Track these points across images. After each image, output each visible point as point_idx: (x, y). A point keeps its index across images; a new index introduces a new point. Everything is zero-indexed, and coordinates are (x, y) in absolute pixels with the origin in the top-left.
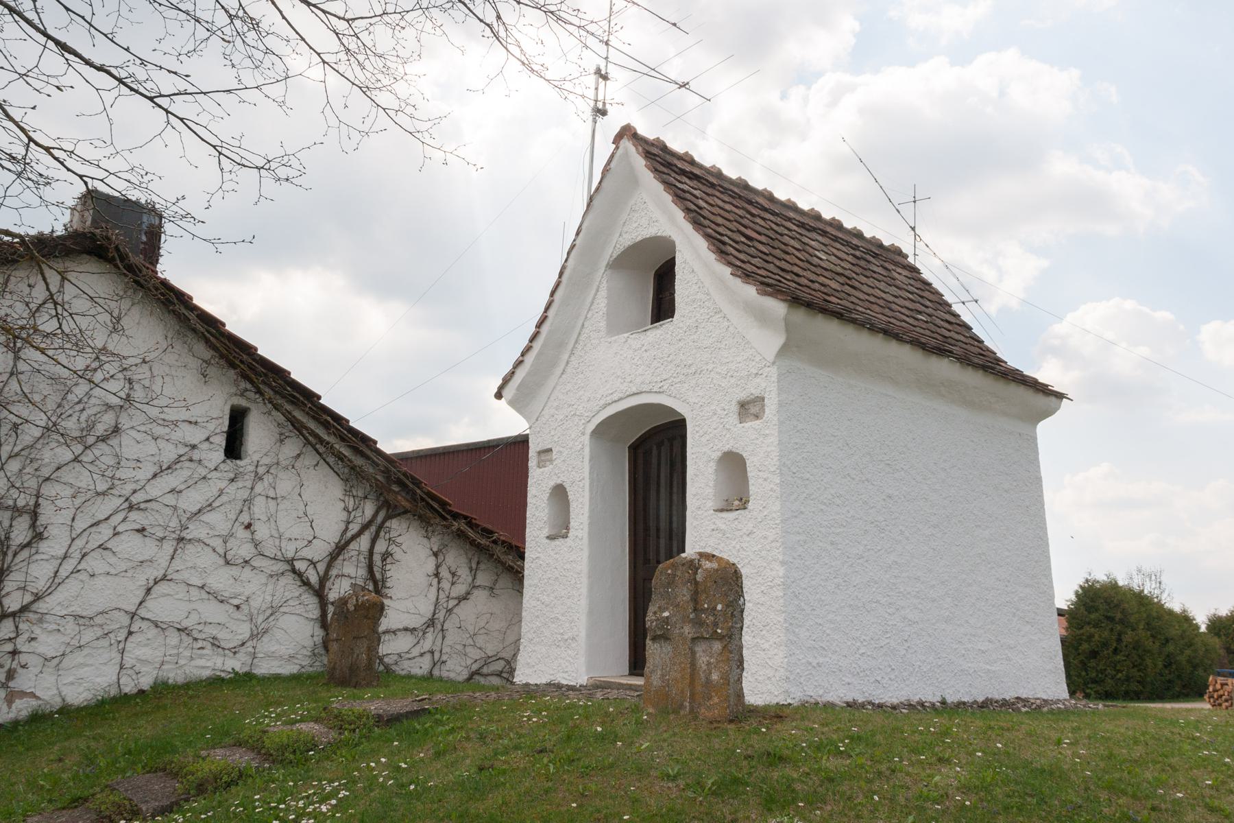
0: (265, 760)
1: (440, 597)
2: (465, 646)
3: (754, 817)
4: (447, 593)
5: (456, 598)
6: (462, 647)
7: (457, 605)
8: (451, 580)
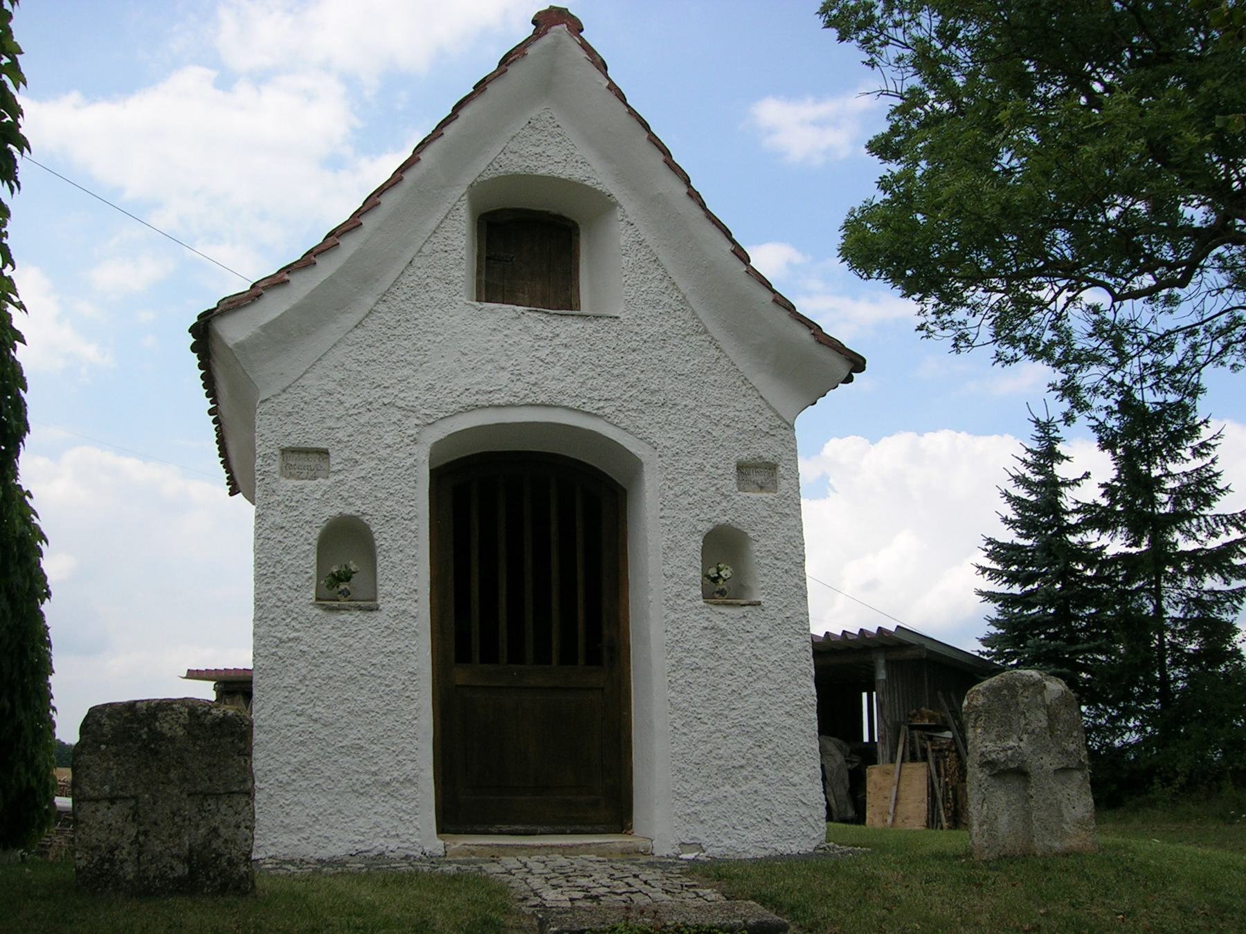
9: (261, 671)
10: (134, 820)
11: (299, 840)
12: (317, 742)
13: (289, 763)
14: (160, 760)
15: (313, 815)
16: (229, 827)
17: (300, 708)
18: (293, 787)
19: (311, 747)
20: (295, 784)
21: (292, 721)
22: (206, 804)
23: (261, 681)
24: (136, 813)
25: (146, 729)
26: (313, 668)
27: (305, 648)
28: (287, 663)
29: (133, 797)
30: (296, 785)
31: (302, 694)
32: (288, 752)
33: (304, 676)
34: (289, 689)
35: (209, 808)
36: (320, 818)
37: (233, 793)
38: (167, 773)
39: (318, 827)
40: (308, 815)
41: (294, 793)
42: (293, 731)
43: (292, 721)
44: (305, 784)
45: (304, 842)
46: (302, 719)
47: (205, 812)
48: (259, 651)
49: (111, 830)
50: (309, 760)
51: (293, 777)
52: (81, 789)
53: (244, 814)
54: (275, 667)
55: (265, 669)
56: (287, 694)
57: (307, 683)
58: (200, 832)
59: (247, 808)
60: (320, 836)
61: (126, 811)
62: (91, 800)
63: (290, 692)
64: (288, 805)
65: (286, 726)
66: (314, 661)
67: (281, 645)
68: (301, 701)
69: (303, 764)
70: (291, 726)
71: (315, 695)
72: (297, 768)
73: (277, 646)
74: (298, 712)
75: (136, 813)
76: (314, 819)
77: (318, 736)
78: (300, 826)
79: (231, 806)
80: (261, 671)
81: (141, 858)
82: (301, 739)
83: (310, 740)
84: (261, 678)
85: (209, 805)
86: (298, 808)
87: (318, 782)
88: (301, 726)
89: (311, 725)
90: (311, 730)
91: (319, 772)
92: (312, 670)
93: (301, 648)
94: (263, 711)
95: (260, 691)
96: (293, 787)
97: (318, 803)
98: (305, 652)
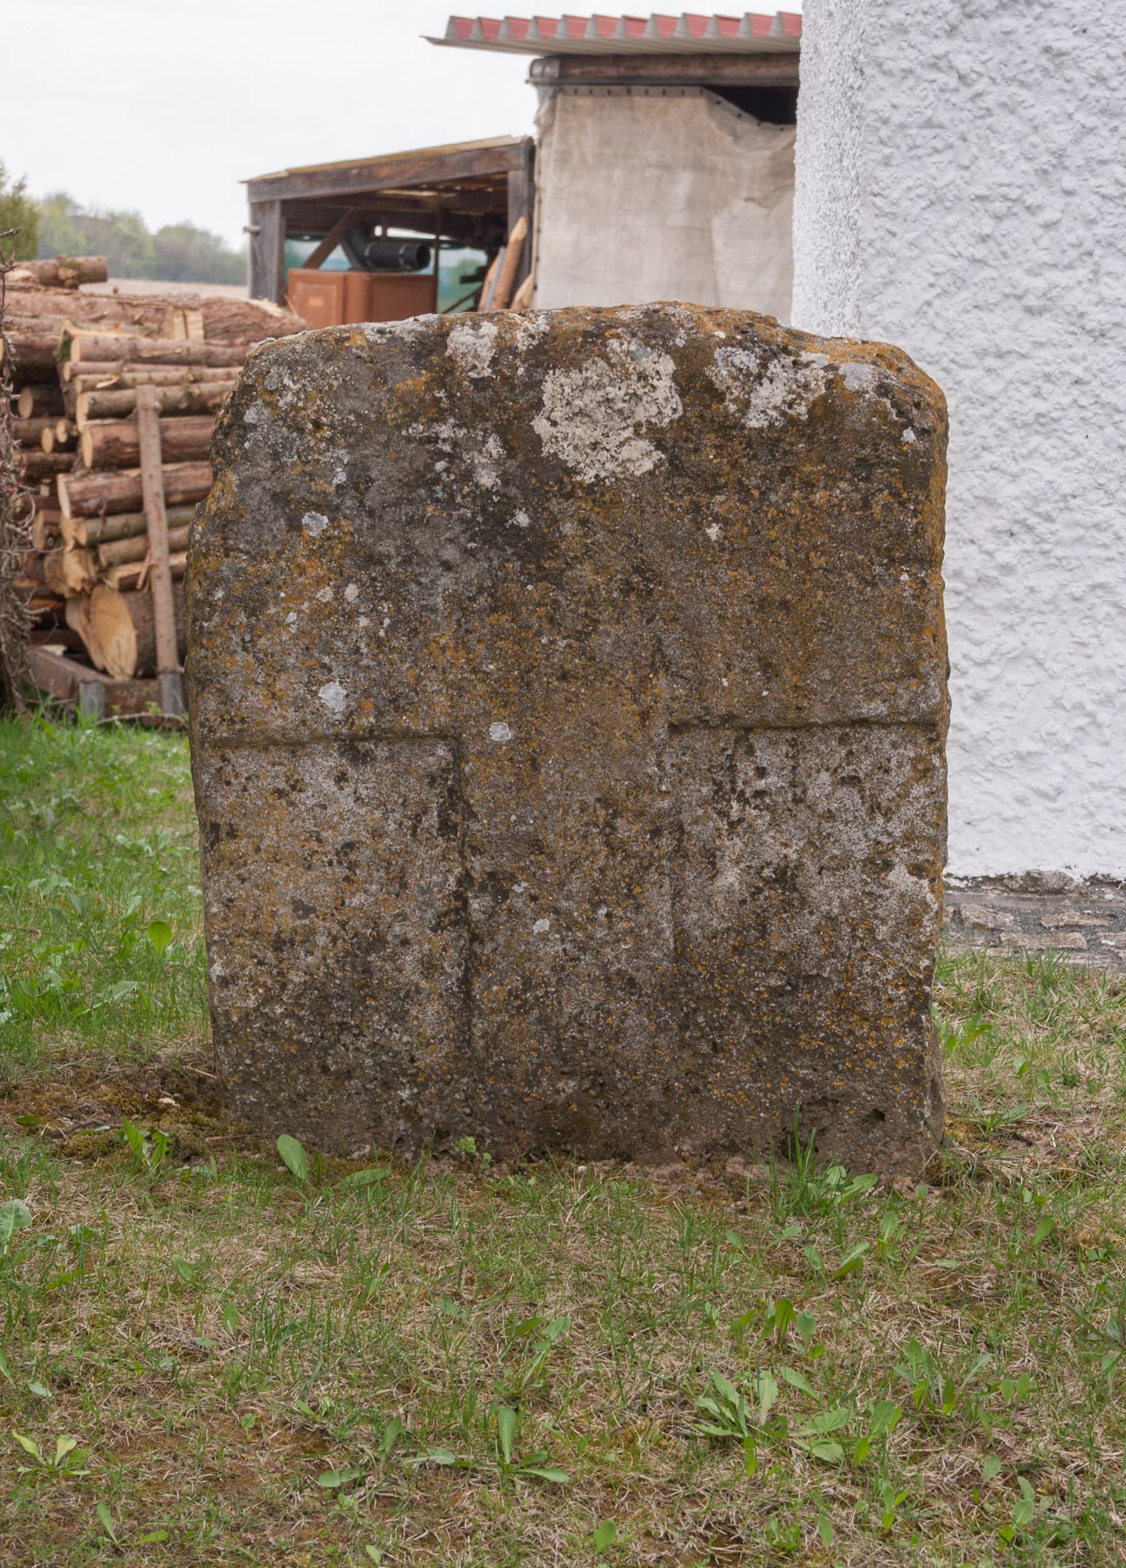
9: (884, 133)
10: (446, 827)
11: (1021, 801)
12: (1101, 420)
13: (990, 503)
14: (556, 580)
15: (1080, 706)
16: (842, 864)
17: (1039, 283)
18: (1001, 595)
19: (1077, 439)
20: (1010, 581)
21: (1005, 333)
22: (746, 768)
23: (883, 174)
24: (454, 797)
25: (493, 446)
26: (1092, 121)
27: (1064, 40)
28: (989, 101)
29: (442, 735)
30: (1016, 585)
31: (1047, 226)
32: (987, 458)
33: (1060, 155)
34: (999, 207)
35: (761, 784)
36: (1103, 716)
37: (864, 722)
38: (581, 636)
39: (1095, 752)
40: (1058, 704)
41: (1007, 618)
42: (1008, 374)
43: (1005, 333)
44: (1047, 583)
45: (1038, 805)
46: (1042, 327)
47: (742, 798)
48: (882, 51)
49: (352, 866)
50: (1067, 489)
51: (1003, 557)
52: (225, 698)
53: (908, 811)
54: (943, 117)
55: (902, 126)
56: (987, 226)
57: (1069, 182)
58: (722, 882)
59: (918, 790)
60: (1100, 786)
61: (416, 790)
62: (269, 743)
63: (998, 218)
64: (982, 664)
65: (983, 353)
66: (1100, 92)
67: (966, 27)
68: (1046, 258)
69: (1044, 507)
70: (1000, 356)
71: (1100, 230)
72: (1022, 523)
73: (952, 31)
74: (1031, 301)
75: (454, 797)
76: (1082, 721)
77: (1107, 396)
78: (1026, 746)
79: (853, 781)
80: (884, 133)
81: (477, 985)
82: (1040, 406)
83: (1073, 413)
84: (887, 162)
85: (761, 772)
86: (1019, 676)
87: (1099, 578)
88: (1046, 354)
89: (1079, 350)
90: (1077, 370)
91: (1106, 537)
92: (1092, 130)
93: (1049, 36)
94: (890, 295)
95: (881, 214)
96: (1001, 595)
97: (1100, 660)
98: (1061, 54)
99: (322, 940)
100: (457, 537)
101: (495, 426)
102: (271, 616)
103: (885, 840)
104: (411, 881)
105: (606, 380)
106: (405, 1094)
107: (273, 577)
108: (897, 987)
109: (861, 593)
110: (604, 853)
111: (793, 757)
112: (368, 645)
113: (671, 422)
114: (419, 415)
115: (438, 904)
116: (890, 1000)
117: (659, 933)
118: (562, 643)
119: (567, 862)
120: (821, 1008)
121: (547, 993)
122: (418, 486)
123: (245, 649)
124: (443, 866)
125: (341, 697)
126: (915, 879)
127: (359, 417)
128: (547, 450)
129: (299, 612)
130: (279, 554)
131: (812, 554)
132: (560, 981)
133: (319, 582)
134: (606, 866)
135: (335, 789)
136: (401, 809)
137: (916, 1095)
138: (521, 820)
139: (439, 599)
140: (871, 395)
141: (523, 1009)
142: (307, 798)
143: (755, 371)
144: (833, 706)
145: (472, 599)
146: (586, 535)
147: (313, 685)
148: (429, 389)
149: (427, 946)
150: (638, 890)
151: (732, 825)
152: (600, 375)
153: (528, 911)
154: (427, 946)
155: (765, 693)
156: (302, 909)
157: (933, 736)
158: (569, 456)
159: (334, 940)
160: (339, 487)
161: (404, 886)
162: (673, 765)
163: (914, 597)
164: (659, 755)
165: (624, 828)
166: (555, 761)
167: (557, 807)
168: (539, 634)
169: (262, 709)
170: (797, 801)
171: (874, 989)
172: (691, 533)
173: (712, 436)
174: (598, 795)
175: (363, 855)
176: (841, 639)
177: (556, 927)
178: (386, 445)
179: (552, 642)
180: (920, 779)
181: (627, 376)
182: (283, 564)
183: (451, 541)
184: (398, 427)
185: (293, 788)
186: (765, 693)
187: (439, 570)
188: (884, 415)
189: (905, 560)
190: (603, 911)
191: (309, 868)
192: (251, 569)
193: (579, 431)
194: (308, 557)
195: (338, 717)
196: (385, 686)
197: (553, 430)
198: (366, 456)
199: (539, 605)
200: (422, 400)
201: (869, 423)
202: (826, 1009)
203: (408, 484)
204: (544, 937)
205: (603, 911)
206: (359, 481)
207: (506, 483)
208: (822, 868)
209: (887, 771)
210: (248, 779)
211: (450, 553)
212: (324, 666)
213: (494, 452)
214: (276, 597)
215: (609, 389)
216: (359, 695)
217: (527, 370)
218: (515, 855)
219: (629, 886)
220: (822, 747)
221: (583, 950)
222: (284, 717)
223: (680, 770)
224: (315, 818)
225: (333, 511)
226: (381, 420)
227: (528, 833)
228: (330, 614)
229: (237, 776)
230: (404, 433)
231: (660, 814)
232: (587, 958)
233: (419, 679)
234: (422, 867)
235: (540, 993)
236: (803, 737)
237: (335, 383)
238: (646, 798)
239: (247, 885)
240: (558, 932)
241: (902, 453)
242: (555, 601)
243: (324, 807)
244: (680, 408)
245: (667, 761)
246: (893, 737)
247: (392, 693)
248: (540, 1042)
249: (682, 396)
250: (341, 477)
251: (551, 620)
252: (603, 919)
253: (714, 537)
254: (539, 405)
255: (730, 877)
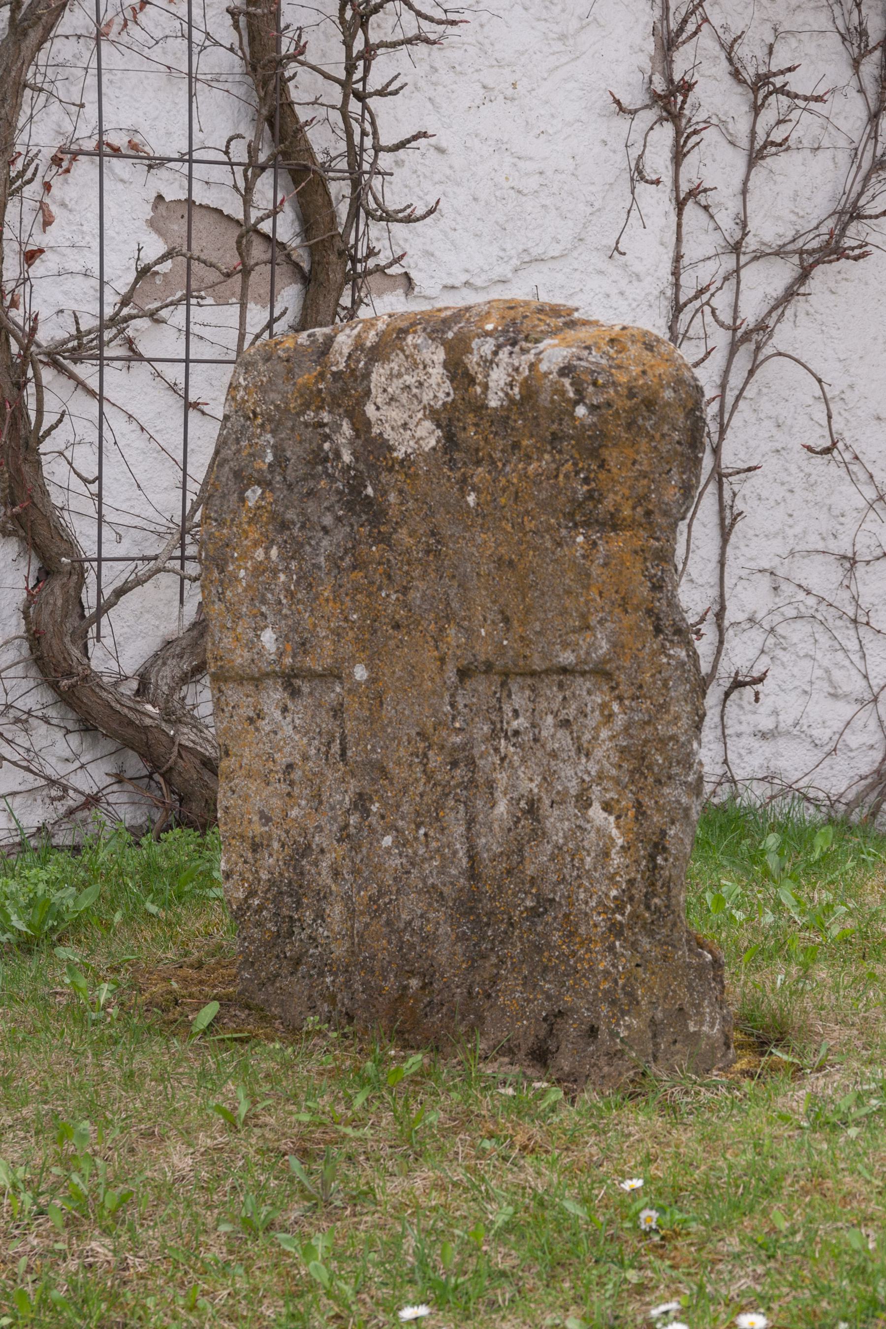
0: (430, 1288)
1: (690, 252)
2: (850, 561)
3: (538, 623)
4: (726, 220)
5: (780, 252)
6: (836, 574)
7: (790, 294)
8: (742, 128)
99: (276, 845)
100: (332, 506)
101: (346, 411)
102: (231, 573)
103: (587, 778)
104: (324, 798)
105: (403, 370)
106: (328, 980)
107: (230, 540)
108: (599, 914)
109: (553, 553)
110: (423, 781)
111: (533, 701)
112: (286, 597)
113: (444, 404)
114: (310, 404)
115: (340, 819)
116: (595, 926)
117: (455, 853)
118: (394, 597)
119: (400, 787)
120: (555, 929)
121: (391, 900)
122: (317, 464)
123: (220, 600)
124: (343, 787)
125: (273, 640)
126: (605, 815)
127: (277, 407)
128: (375, 430)
129: (246, 569)
130: (233, 520)
131: (526, 519)
132: (398, 890)
133: (256, 544)
134: (424, 792)
135: (280, 718)
136: (318, 737)
137: (614, 1015)
138: (374, 750)
139: (322, 559)
140: (553, 377)
141: (376, 914)
142: (265, 725)
143: (489, 357)
144: (545, 656)
145: (342, 559)
146: (402, 504)
147: (258, 630)
148: (317, 382)
149: (334, 855)
150: (441, 814)
151: (503, 759)
152: (399, 366)
153: (379, 829)
154: (334, 855)
155: (505, 643)
156: (266, 819)
157: (613, 684)
158: (390, 435)
159: (283, 846)
160: (270, 465)
161: (321, 803)
162: (466, 706)
163: (584, 557)
164: (452, 696)
165: (435, 760)
166: (392, 700)
167: (394, 739)
168: (380, 589)
169: (230, 650)
170: (536, 740)
171: (586, 914)
172: (458, 501)
173: (471, 415)
174: (418, 729)
175: (297, 775)
176: (543, 594)
177: (396, 843)
178: (293, 429)
179: (388, 596)
180: (605, 724)
181: (416, 366)
182: (235, 529)
183: (328, 509)
184: (298, 414)
185: (258, 715)
186: (505, 643)
187: (321, 534)
188: (563, 393)
189: (587, 524)
190: (422, 831)
191: (268, 784)
192: (217, 534)
193: (394, 414)
194: (249, 523)
195: (273, 657)
196: (296, 631)
197: (378, 414)
198: (282, 439)
199: (379, 564)
200: (311, 392)
201: (552, 401)
202: (559, 931)
203: (309, 462)
204: (388, 851)
205: (422, 831)
206: (280, 461)
207: (357, 459)
208: (553, 802)
209: (586, 716)
210: (233, 707)
211: (328, 520)
212: (262, 614)
213: (347, 433)
214: (232, 557)
215: (406, 377)
216: (282, 638)
217: (366, 364)
218: (372, 779)
219: (436, 810)
220: (548, 692)
221: (413, 864)
222: (242, 656)
223: (471, 710)
224: (271, 742)
225: (266, 484)
226: (287, 410)
227: (378, 761)
228: (264, 571)
229: (227, 705)
230: (302, 419)
231: (455, 749)
232: (415, 872)
233: (315, 626)
234: (330, 787)
235: (387, 900)
236: (566, 679)
237: (265, 379)
238: (444, 734)
239: (235, 796)
240: (397, 847)
241: (575, 428)
242: (389, 561)
243: (275, 733)
244: (452, 392)
245: (461, 702)
246: (588, 685)
247: (301, 638)
248: (389, 943)
249: (452, 381)
250: (270, 458)
251: (389, 577)
252: (422, 838)
253: (472, 504)
254: (368, 393)
255: (502, 807)
